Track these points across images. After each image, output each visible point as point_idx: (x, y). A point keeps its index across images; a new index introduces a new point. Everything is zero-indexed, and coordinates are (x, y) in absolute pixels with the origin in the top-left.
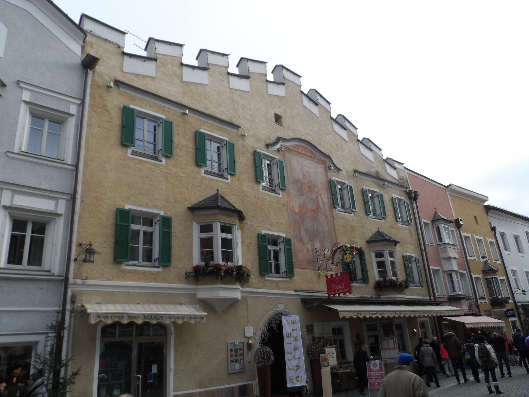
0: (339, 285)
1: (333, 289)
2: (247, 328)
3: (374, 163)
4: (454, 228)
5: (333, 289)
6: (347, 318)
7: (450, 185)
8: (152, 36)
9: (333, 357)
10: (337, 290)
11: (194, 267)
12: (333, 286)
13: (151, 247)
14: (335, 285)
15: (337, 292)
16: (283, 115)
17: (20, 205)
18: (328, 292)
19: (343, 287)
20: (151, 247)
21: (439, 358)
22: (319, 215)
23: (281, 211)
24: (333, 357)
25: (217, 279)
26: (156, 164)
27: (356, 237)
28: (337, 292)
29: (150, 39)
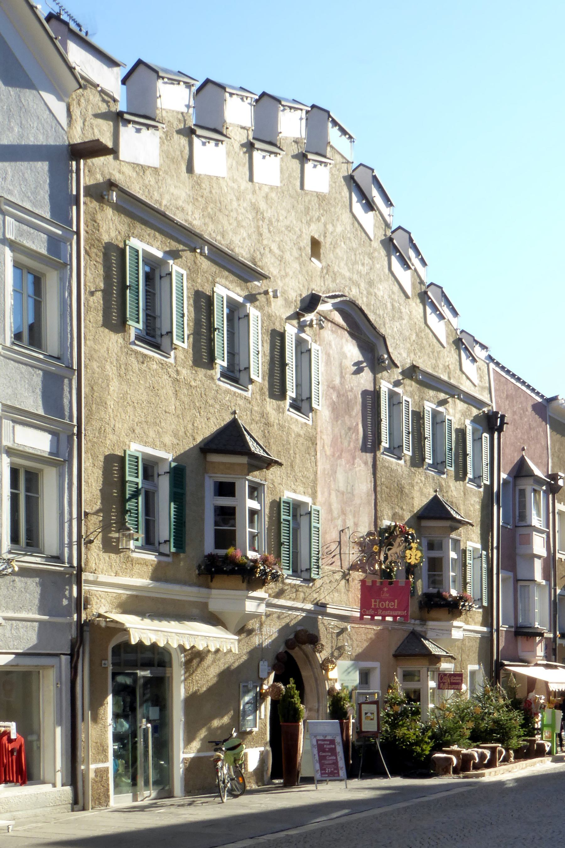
0: (387, 602)
1: (373, 607)
2: (261, 663)
3: (444, 347)
4: (481, 426)
5: (373, 607)
6: (152, 587)
7: (555, 398)
8: (145, 60)
9: (372, 719)
10: (381, 609)
11: (206, 556)
12: (373, 600)
13: (148, 518)
14: (378, 600)
15: (380, 612)
16: (321, 239)
17: (158, 506)
18: (361, 609)
19: (396, 607)
20: (148, 518)
21: (128, 675)
22: (356, 461)
23: (309, 454)
24: (372, 719)
25: (243, 582)
26: (163, 362)
27: (404, 507)
28: (380, 612)
29: (140, 63)
